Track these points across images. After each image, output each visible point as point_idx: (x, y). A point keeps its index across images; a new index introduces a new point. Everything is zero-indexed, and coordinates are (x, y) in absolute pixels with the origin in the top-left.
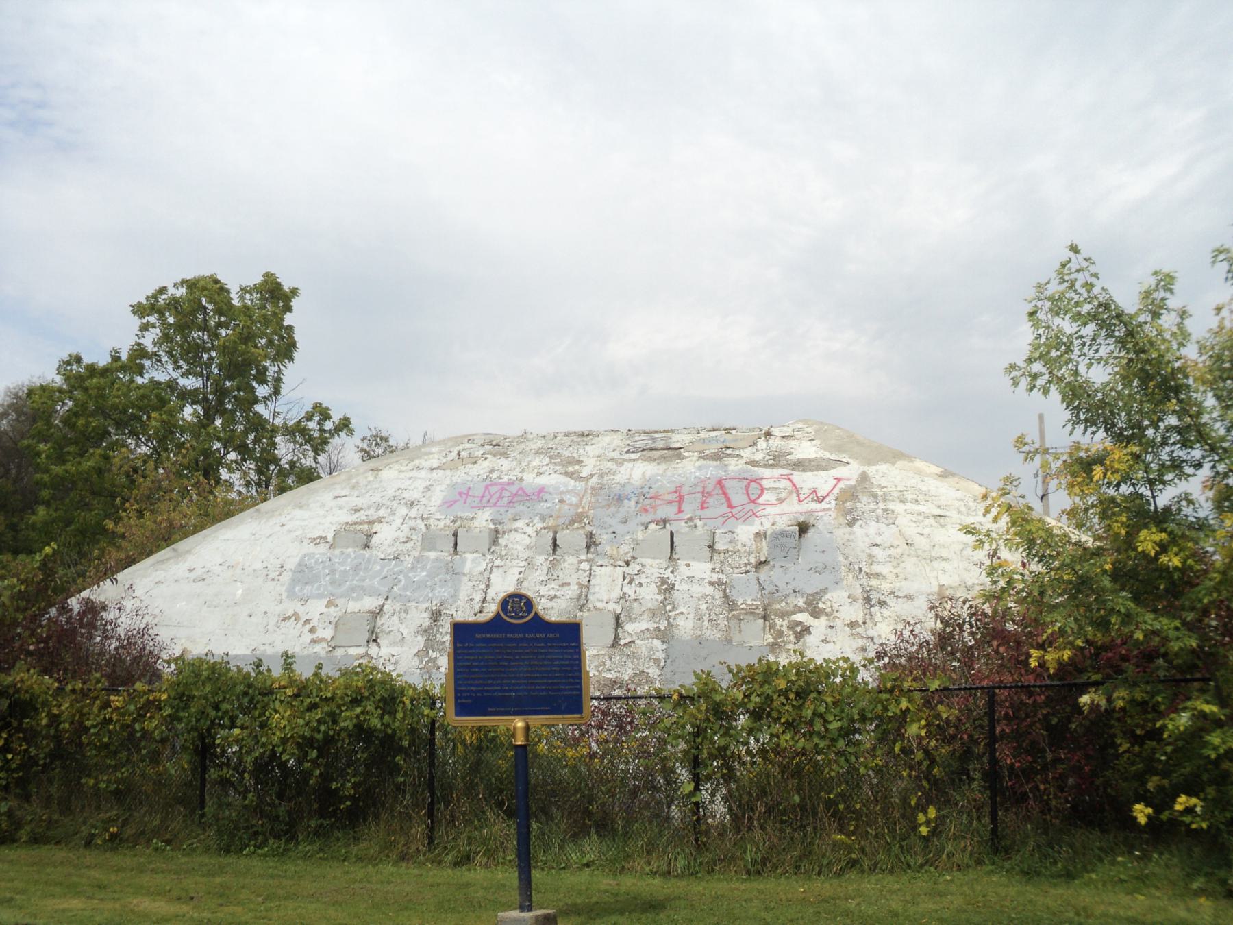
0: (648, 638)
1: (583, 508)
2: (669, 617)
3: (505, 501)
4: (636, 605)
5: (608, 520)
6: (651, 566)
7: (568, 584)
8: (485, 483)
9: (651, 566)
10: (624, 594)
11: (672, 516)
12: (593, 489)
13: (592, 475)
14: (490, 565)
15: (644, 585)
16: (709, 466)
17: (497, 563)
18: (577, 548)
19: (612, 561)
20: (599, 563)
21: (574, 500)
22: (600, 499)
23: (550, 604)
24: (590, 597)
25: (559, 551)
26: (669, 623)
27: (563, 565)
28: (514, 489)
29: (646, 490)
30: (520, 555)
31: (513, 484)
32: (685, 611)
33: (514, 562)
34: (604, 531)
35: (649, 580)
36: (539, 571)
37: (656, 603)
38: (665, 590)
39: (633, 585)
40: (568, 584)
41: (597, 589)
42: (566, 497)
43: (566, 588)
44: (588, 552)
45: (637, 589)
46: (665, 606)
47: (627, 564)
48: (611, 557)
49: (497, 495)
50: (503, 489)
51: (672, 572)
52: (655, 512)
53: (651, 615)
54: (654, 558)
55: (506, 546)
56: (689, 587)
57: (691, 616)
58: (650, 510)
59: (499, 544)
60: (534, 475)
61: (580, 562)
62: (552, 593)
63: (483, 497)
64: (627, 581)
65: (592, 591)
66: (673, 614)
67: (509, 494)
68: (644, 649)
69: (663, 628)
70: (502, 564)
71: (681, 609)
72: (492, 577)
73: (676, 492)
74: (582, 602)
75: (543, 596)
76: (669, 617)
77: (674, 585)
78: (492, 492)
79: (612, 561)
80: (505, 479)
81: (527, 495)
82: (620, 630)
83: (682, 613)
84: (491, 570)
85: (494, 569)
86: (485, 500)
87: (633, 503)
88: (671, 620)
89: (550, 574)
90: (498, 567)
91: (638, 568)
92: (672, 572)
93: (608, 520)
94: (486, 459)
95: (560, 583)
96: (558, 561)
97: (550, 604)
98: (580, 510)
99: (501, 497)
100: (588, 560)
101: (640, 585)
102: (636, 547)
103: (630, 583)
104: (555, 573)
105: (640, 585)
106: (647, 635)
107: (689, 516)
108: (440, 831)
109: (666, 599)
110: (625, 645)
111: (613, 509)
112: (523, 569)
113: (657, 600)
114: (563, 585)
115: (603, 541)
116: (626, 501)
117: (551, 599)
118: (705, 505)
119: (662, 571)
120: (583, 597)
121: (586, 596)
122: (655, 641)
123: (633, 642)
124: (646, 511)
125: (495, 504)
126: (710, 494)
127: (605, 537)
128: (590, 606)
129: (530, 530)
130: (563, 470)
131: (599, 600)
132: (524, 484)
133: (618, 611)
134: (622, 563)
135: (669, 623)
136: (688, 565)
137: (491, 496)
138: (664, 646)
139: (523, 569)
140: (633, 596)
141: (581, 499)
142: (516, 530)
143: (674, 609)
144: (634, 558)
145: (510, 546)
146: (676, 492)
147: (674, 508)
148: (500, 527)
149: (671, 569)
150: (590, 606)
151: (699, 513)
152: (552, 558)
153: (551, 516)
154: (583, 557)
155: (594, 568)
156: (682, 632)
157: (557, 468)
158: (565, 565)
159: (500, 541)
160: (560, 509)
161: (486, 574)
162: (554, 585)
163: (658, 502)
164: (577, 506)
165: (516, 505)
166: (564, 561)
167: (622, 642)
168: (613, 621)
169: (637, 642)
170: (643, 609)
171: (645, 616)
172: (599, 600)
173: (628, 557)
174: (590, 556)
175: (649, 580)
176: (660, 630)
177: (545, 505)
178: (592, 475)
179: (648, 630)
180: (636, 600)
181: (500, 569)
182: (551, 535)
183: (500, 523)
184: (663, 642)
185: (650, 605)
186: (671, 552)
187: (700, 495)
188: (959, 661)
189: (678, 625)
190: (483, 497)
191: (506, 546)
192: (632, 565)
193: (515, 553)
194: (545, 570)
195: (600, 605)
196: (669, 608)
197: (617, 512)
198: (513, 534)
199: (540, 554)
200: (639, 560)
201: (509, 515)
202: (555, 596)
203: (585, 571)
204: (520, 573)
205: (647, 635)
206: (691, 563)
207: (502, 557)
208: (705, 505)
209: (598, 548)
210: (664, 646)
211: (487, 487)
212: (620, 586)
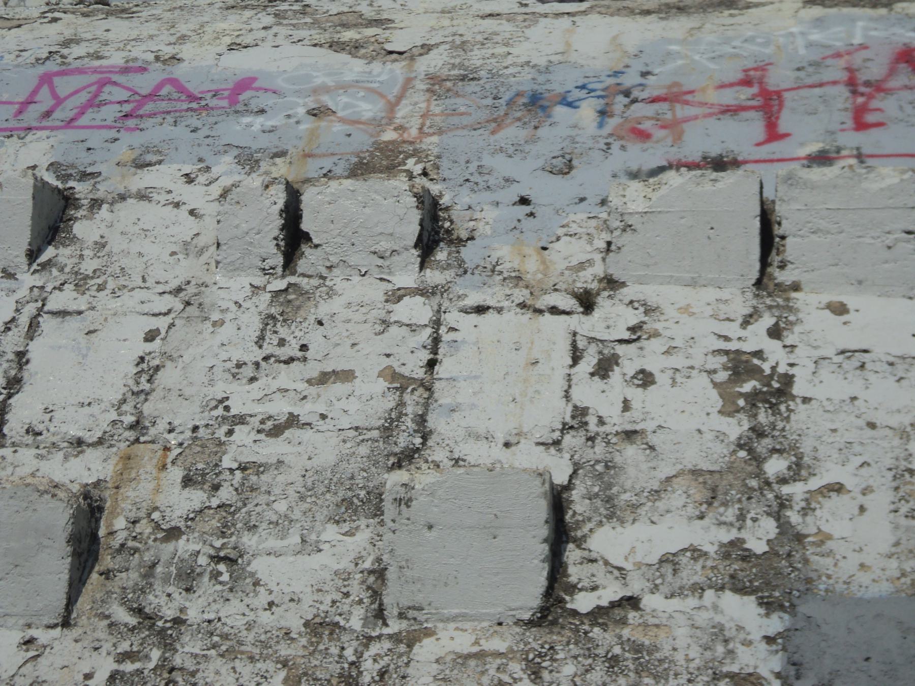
0: (698, 589)
1: (400, 128)
2: (783, 503)
3: (110, 113)
4: (631, 452)
5: (502, 166)
6: (686, 310)
7: (347, 376)
8: (41, 70)
9: (686, 310)
10: (580, 412)
11: (745, 150)
12: (434, 80)
13: (427, 48)
14: (30, 309)
15: (662, 379)
16: (853, 20)
17: (56, 302)
18: (384, 245)
19: (521, 294)
20: (474, 299)
21: (368, 109)
22: (460, 104)
23: (271, 449)
24: (434, 421)
25: (309, 259)
26: (784, 526)
27: (324, 309)
28: (144, 83)
29: (630, 79)
30: (156, 273)
31: (143, 70)
32: (849, 482)
33: (129, 300)
34: (487, 196)
35: (677, 361)
36: (226, 332)
37: (721, 450)
38: (753, 398)
39: (616, 375)
40: (347, 376)
41: (464, 394)
42: (338, 102)
43: (338, 389)
44: (422, 266)
45: (636, 395)
46: (757, 460)
47: (587, 302)
48: (518, 279)
49: (83, 97)
50: (102, 84)
51: (775, 333)
52: (678, 138)
53: (699, 493)
54: (693, 284)
55: (101, 245)
56: (854, 386)
57: (882, 499)
58: (659, 134)
59: (74, 239)
60: (223, 48)
61: (396, 296)
62: (280, 408)
63: (29, 102)
64: (589, 362)
65: (444, 395)
66: (796, 490)
67: (124, 95)
68: (682, 633)
69: (758, 547)
70: (82, 303)
71: (828, 475)
72: (36, 350)
73: (746, 82)
74: (403, 441)
75: (241, 420)
76: (783, 503)
77: (788, 380)
78: (62, 92)
79: (521, 294)
80: (116, 59)
81: (192, 98)
82: (572, 554)
83: (838, 488)
84: (33, 326)
85: (46, 322)
86: (33, 112)
87: (587, 112)
88: (793, 517)
89: (271, 339)
90: (63, 314)
91: (633, 317)
92: (775, 333)
93: (502, 166)
94: (55, 20)
95: (313, 370)
96: (305, 295)
97: (271, 449)
98: (389, 135)
99: (93, 103)
100: (423, 292)
101: (645, 379)
102: (619, 239)
103: (604, 369)
104: (293, 335)
105: (645, 379)
106: (692, 573)
107: (813, 148)
108: (685, 89)
109: (759, 432)
110: (598, 615)
111: (512, 133)
112: (162, 323)
113: (720, 436)
114: (324, 378)
115: (483, 229)
116: (560, 111)
117: (276, 431)
118: (870, 118)
119: (733, 330)
120: (409, 423)
121: (421, 420)
122: (729, 599)
123: (632, 602)
124: (644, 136)
125: (69, 124)
126: (878, 87)
127: (490, 214)
128: (439, 455)
129: (194, 196)
130: (323, 38)
131: (474, 435)
132: (179, 71)
133: (560, 478)
134: (565, 302)
135: (784, 526)
136: (840, 309)
137: (59, 101)
138: (776, 624)
139: (162, 323)
140: (617, 421)
141: (392, 107)
142: (143, 196)
143: (797, 471)
144: (611, 283)
145: (116, 244)
146: (746, 82)
147: (755, 126)
148: (81, 189)
149: (768, 321)
150: (439, 455)
151: (851, 139)
152: (281, 284)
153: (282, 154)
154: (407, 278)
155: (452, 317)
156: (849, 567)
157: (303, 33)
158: (335, 305)
159: (78, 228)
160: (313, 134)
161: (13, 341)
162: (289, 377)
163: (681, 111)
164: (378, 124)
165: (148, 123)
166: (331, 293)
167: (583, 603)
168: (541, 510)
169: (650, 601)
170: (666, 470)
171: (676, 499)
172: (474, 435)
173: (587, 280)
174: (433, 277)
175: (677, 361)
176: (747, 556)
177: (259, 122)
178: (427, 48)
179: (696, 553)
180: (630, 435)
181: (72, 323)
182: (279, 196)
183: (84, 176)
184: (769, 606)
185: (693, 457)
186: (765, 262)
187: (842, 92)
188: (533, 659)
189: (824, 538)
190: (29, 102)
191: (101, 245)
192: (604, 306)
193: (136, 268)
194: (252, 323)
195: (474, 452)
196: (775, 466)
197: (533, 140)
198: (130, 210)
199: (235, 269)
200: (627, 293)
201: (123, 150)
202: (293, 421)
203: (413, 328)
204: (150, 337)
205: (692, 573)
206: (851, 301)
207: (81, 282)
208: (870, 118)
209: (468, 253)
210: (776, 624)
211: (46, 79)
212: (559, 384)
